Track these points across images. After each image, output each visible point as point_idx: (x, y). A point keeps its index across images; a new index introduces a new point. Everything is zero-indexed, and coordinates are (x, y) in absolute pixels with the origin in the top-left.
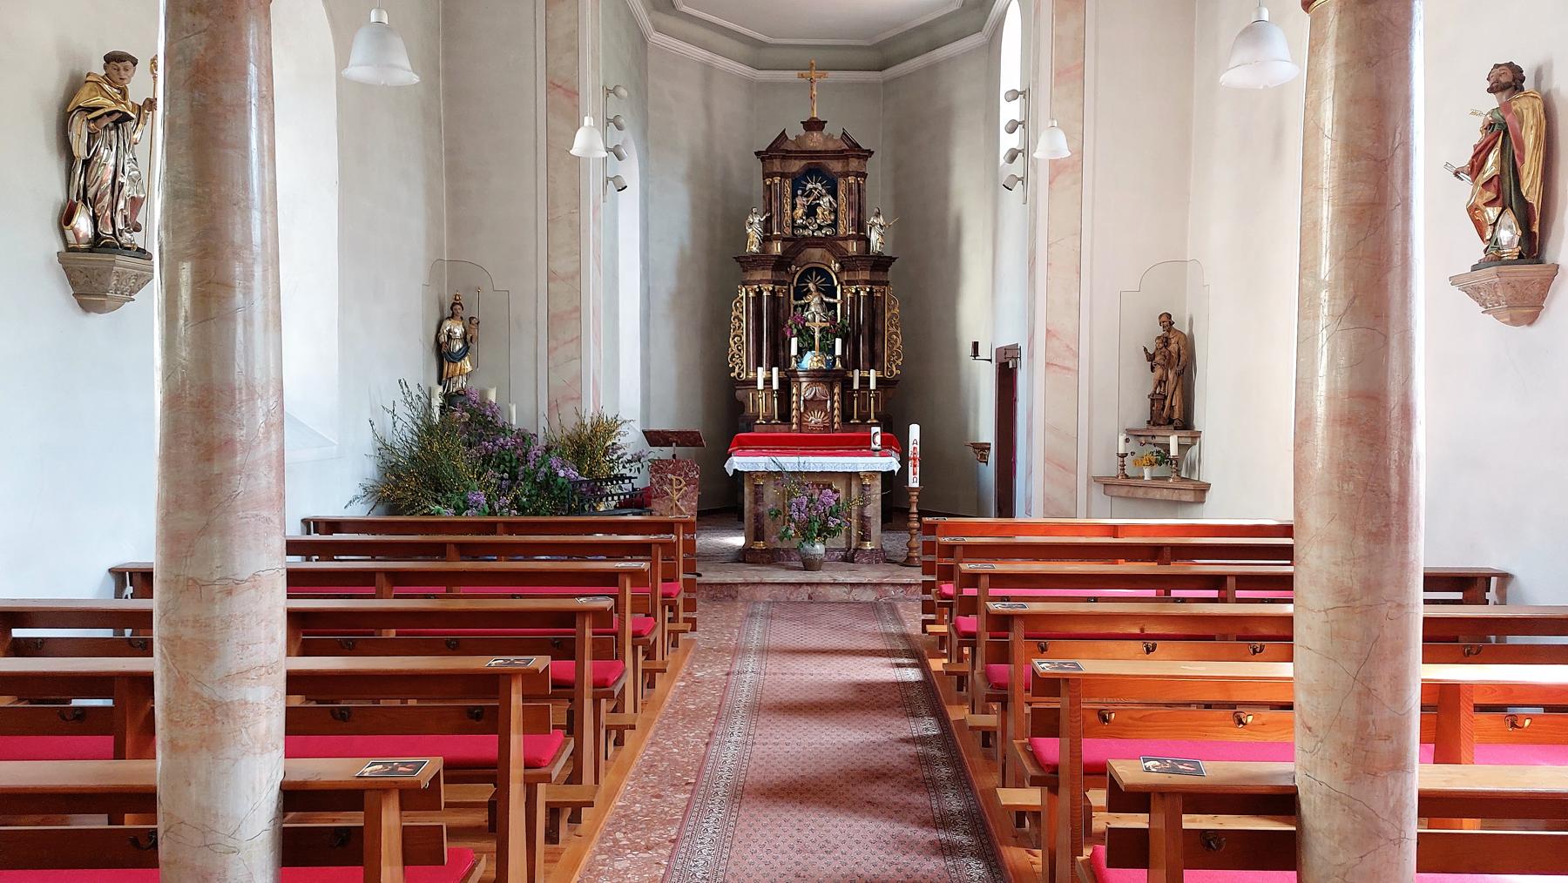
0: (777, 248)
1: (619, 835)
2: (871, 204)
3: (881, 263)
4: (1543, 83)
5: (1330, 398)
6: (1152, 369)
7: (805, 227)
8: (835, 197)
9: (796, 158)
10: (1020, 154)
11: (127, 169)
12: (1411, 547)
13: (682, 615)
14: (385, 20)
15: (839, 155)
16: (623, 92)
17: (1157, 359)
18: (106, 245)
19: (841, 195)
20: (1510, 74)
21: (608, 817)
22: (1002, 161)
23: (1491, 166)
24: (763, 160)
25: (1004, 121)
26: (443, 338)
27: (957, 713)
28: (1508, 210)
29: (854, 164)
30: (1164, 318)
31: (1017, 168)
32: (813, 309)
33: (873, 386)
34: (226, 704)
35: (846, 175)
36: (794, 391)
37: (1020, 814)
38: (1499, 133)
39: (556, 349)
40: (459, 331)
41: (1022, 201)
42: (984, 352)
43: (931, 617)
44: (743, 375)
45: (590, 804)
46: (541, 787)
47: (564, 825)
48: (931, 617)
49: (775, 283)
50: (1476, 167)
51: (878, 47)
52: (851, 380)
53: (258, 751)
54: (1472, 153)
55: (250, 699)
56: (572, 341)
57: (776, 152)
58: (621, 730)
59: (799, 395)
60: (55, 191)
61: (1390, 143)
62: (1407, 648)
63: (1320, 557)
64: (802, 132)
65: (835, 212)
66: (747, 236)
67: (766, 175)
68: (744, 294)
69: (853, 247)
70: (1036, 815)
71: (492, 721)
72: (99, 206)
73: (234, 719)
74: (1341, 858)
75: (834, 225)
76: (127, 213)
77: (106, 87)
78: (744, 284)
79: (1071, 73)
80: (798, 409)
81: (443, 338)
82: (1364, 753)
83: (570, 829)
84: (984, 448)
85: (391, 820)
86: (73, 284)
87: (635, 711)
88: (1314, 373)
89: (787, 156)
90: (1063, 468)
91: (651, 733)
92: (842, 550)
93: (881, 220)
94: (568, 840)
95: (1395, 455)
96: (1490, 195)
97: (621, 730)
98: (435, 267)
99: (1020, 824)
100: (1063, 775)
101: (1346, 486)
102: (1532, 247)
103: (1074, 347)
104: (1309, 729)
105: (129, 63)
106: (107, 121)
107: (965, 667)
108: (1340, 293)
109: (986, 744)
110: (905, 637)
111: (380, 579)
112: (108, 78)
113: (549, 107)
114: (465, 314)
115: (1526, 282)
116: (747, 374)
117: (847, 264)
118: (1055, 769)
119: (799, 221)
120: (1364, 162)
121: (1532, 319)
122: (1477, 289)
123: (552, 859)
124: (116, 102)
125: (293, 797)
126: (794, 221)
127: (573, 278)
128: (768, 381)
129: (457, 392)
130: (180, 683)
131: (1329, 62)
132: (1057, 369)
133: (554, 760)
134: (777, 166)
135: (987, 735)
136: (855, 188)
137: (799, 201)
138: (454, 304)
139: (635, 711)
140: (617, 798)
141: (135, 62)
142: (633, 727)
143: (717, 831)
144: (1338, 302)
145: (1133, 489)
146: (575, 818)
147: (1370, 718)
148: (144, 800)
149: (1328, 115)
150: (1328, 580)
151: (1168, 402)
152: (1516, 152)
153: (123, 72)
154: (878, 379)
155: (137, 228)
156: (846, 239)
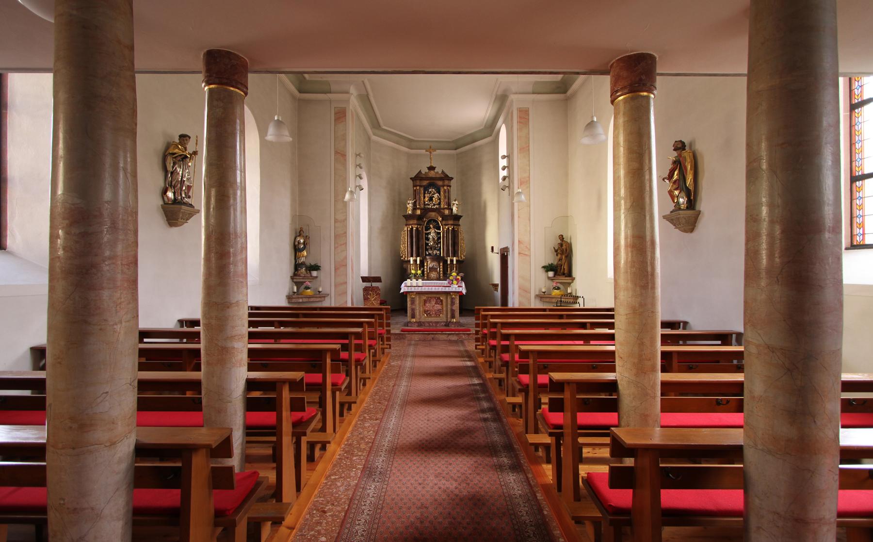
0: (418, 212)
1: (365, 415)
2: (452, 197)
3: (457, 218)
4: (693, 148)
5: (626, 238)
6: (557, 255)
7: (429, 205)
8: (440, 194)
9: (425, 180)
10: (507, 178)
11: (186, 175)
12: (656, 291)
13: (386, 343)
14: (280, 119)
15: (441, 179)
16: (362, 155)
17: (558, 251)
18: (178, 202)
19: (442, 193)
20: (680, 143)
21: (361, 409)
22: (501, 181)
23: (675, 177)
24: (413, 181)
25: (501, 166)
26: (296, 243)
27: (489, 375)
28: (683, 192)
29: (446, 182)
30: (561, 236)
31: (506, 183)
32: (432, 234)
33: (455, 262)
34: (227, 348)
35: (443, 186)
36: (425, 264)
37: (514, 405)
38: (678, 164)
39: (337, 247)
40: (302, 241)
41: (508, 194)
42: (495, 250)
43: (479, 343)
44: (406, 259)
45: (355, 403)
46: (338, 393)
47: (345, 411)
48: (479, 343)
49: (418, 225)
50: (670, 176)
51: (454, 142)
52: (447, 261)
53: (238, 366)
54: (668, 172)
55: (235, 347)
56: (343, 244)
57: (417, 178)
58: (365, 379)
59: (427, 266)
60: (161, 183)
61: (644, 148)
62: (656, 327)
63: (624, 296)
64: (427, 171)
65: (440, 199)
66: (407, 208)
67: (414, 186)
68: (406, 229)
69: (447, 212)
70: (520, 405)
71: (319, 368)
72: (176, 188)
73: (230, 354)
74: (634, 404)
75: (440, 204)
76: (186, 191)
77: (180, 146)
78: (406, 225)
79: (525, 149)
80: (427, 271)
81: (296, 243)
82: (641, 365)
83: (348, 413)
84: (496, 286)
85: (286, 395)
86: (167, 216)
87: (370, 373)
88: (620, 229)
89: (422, 179)
90: (526, 291)
91: (376, 382)
92: (445, 322)
93: (457, 202)
94: (347, 416)
95: (649, 258)
96: (675, 186)
97: (365, 379)
98: (294, 217)
99: (514, 410)
100: (531, 388)
101: (632, 269)
102: (692, 204)
103: (528, 247)
104: (621, 358)
105: (188, 138)
106: (179, 158)
107: (493, 359)
108: (628, 201)
109: (500, 385)
110: (467, 351)
111: (276, 324)
112: (180, 143)
113: (336, 160)
114: (304, 235)
115: (689, 217)
116: (408, 258)
117: (445, 218)
118: (527, 385)
119: (426, 203)
120: (635, 155)
121: (692, 230)
122: (672, 220)
123: (342, 422)
124: (183, 152)
125: (251, 385)
126: (424, 202)
127: (344, 221)
128: (415, 261)
129: (301, 263)
130: (210, 340)
131: (621, 120)
132: (523, 255)
133: (343, 383)
134: (418, 183)
135: (500, 381)
136: (447, 190)
137: (426, 195)
138: (300, 231)
139: (370, 373)
140: (364, 403)
141: (190, 137)
142: (369, 378)
143: (375, 495)
144: (628, 204)
145: (551, 299)
146: (350, 409)
147: (643, 352)
148: (196, 385)
149: (621, 139)
150: (627, 304)
151: (563, 267)
152: (684, 171)
153: (185, 141)
154: (457, 261)
155: (189, 197)
156: (444, 209)
